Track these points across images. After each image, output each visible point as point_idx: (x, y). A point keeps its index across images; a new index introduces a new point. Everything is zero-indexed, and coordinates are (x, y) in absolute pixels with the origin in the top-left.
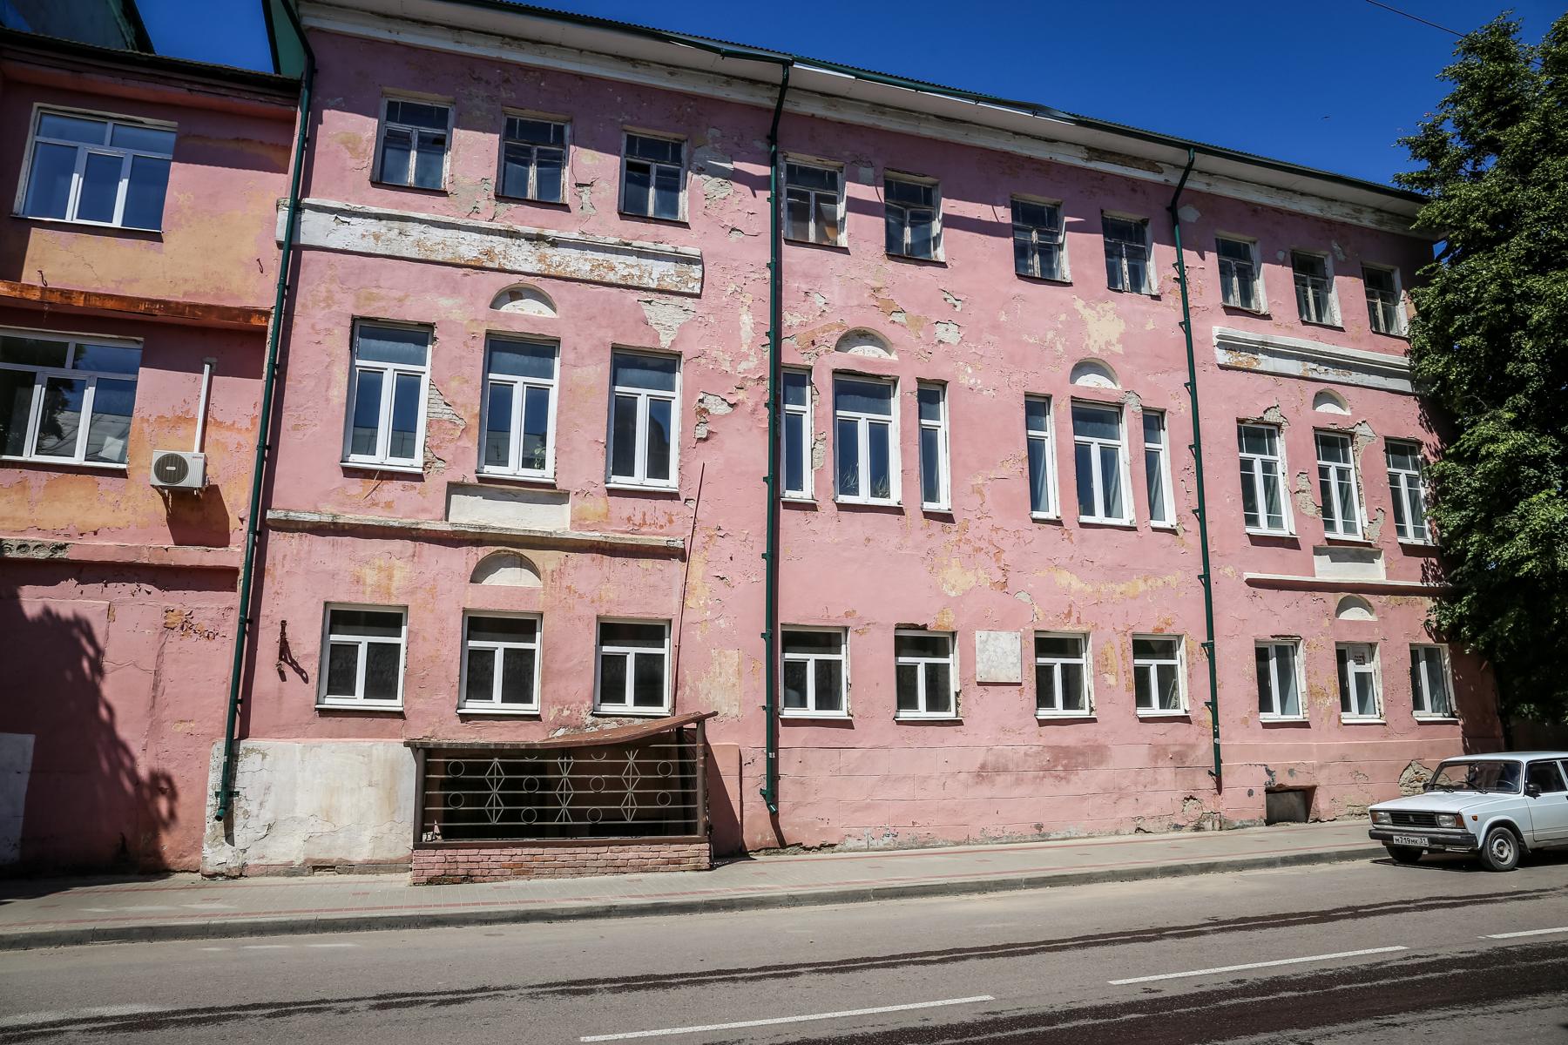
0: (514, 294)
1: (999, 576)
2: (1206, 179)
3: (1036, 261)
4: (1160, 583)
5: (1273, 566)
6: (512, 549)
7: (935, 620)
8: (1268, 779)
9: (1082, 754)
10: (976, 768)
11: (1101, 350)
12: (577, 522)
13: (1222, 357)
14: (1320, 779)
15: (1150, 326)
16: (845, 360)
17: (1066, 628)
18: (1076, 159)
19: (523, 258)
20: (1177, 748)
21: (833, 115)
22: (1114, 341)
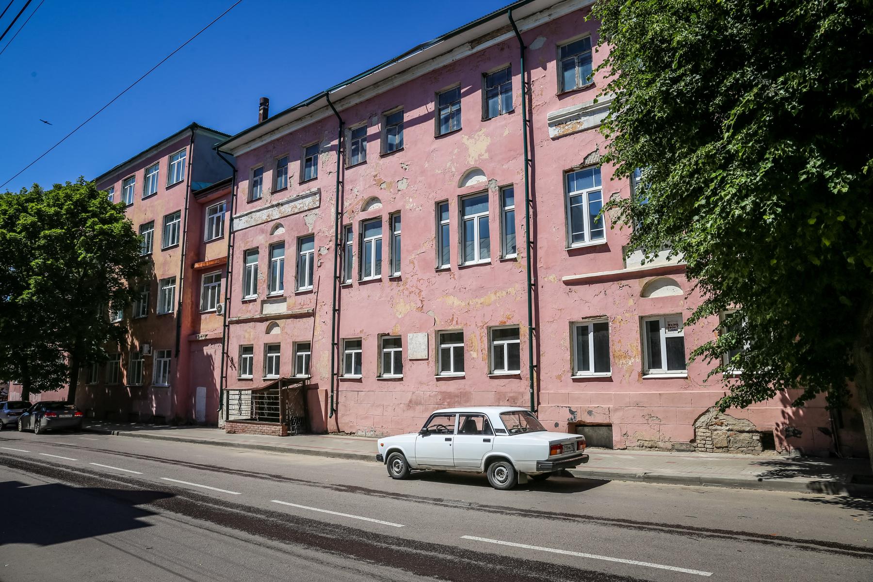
0: (277, 227)
1: (420, 305)
2: (546, 13)
3: (446, 125)
4: (504, 293)
5: (585, 268)
6: (272, 321)
7: (393, 330)
8: (570, 416)
9: (458, 396)
10: (407, 402)
11: (476, 161)
12: (288, 309)
13: (553, 132)
14: (615, 419)
15: (506, 133)
16: (364, 216)
17: (450, 328)
18: (467, 52)
19: (276, 213)
20: (512, 395)
21: (362, 99)
22: (483, 152)
